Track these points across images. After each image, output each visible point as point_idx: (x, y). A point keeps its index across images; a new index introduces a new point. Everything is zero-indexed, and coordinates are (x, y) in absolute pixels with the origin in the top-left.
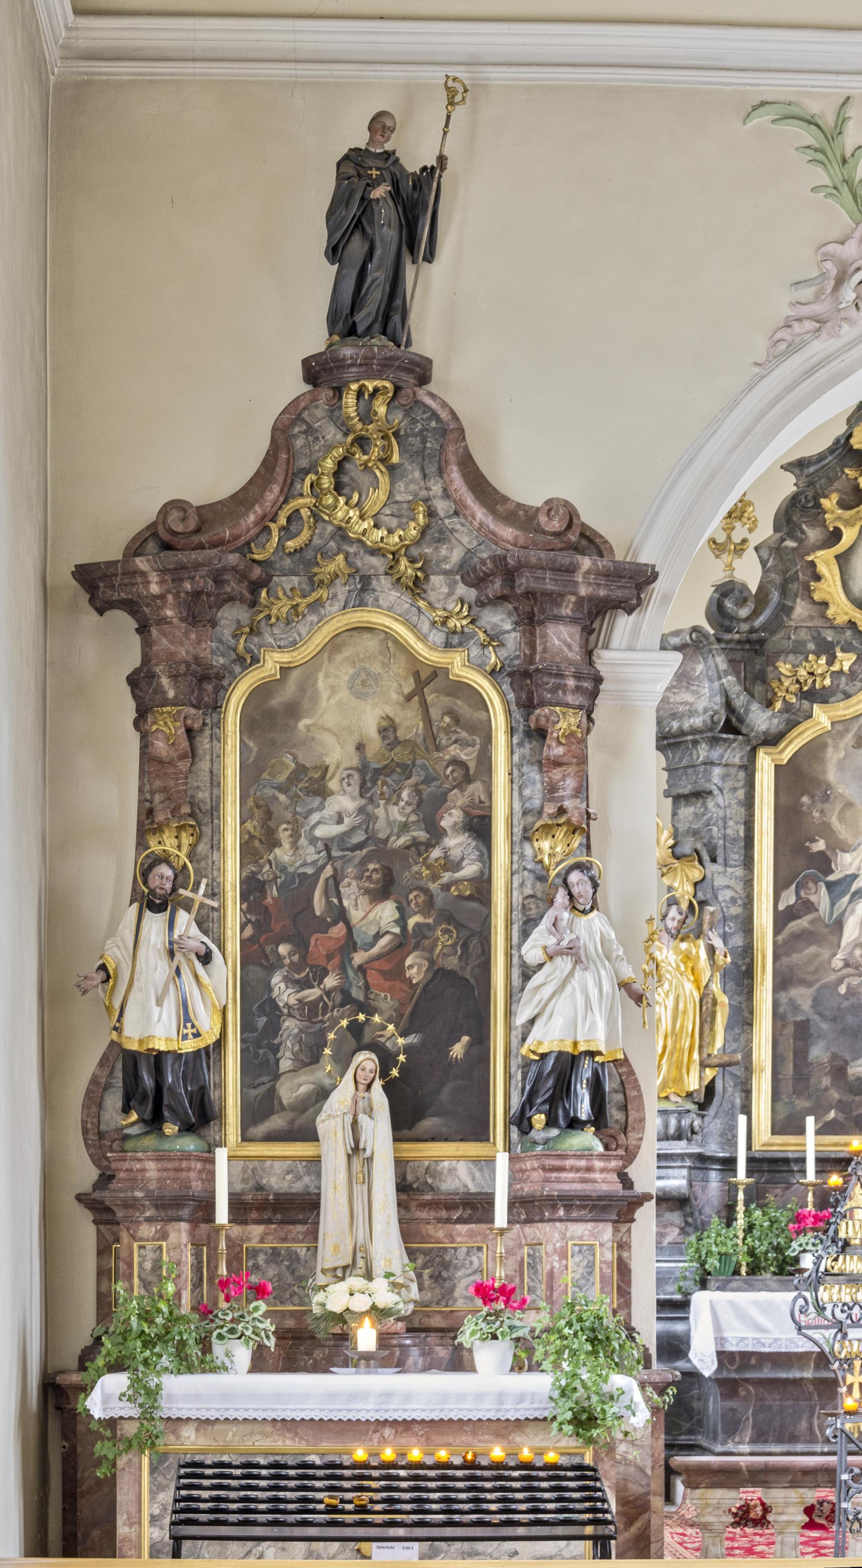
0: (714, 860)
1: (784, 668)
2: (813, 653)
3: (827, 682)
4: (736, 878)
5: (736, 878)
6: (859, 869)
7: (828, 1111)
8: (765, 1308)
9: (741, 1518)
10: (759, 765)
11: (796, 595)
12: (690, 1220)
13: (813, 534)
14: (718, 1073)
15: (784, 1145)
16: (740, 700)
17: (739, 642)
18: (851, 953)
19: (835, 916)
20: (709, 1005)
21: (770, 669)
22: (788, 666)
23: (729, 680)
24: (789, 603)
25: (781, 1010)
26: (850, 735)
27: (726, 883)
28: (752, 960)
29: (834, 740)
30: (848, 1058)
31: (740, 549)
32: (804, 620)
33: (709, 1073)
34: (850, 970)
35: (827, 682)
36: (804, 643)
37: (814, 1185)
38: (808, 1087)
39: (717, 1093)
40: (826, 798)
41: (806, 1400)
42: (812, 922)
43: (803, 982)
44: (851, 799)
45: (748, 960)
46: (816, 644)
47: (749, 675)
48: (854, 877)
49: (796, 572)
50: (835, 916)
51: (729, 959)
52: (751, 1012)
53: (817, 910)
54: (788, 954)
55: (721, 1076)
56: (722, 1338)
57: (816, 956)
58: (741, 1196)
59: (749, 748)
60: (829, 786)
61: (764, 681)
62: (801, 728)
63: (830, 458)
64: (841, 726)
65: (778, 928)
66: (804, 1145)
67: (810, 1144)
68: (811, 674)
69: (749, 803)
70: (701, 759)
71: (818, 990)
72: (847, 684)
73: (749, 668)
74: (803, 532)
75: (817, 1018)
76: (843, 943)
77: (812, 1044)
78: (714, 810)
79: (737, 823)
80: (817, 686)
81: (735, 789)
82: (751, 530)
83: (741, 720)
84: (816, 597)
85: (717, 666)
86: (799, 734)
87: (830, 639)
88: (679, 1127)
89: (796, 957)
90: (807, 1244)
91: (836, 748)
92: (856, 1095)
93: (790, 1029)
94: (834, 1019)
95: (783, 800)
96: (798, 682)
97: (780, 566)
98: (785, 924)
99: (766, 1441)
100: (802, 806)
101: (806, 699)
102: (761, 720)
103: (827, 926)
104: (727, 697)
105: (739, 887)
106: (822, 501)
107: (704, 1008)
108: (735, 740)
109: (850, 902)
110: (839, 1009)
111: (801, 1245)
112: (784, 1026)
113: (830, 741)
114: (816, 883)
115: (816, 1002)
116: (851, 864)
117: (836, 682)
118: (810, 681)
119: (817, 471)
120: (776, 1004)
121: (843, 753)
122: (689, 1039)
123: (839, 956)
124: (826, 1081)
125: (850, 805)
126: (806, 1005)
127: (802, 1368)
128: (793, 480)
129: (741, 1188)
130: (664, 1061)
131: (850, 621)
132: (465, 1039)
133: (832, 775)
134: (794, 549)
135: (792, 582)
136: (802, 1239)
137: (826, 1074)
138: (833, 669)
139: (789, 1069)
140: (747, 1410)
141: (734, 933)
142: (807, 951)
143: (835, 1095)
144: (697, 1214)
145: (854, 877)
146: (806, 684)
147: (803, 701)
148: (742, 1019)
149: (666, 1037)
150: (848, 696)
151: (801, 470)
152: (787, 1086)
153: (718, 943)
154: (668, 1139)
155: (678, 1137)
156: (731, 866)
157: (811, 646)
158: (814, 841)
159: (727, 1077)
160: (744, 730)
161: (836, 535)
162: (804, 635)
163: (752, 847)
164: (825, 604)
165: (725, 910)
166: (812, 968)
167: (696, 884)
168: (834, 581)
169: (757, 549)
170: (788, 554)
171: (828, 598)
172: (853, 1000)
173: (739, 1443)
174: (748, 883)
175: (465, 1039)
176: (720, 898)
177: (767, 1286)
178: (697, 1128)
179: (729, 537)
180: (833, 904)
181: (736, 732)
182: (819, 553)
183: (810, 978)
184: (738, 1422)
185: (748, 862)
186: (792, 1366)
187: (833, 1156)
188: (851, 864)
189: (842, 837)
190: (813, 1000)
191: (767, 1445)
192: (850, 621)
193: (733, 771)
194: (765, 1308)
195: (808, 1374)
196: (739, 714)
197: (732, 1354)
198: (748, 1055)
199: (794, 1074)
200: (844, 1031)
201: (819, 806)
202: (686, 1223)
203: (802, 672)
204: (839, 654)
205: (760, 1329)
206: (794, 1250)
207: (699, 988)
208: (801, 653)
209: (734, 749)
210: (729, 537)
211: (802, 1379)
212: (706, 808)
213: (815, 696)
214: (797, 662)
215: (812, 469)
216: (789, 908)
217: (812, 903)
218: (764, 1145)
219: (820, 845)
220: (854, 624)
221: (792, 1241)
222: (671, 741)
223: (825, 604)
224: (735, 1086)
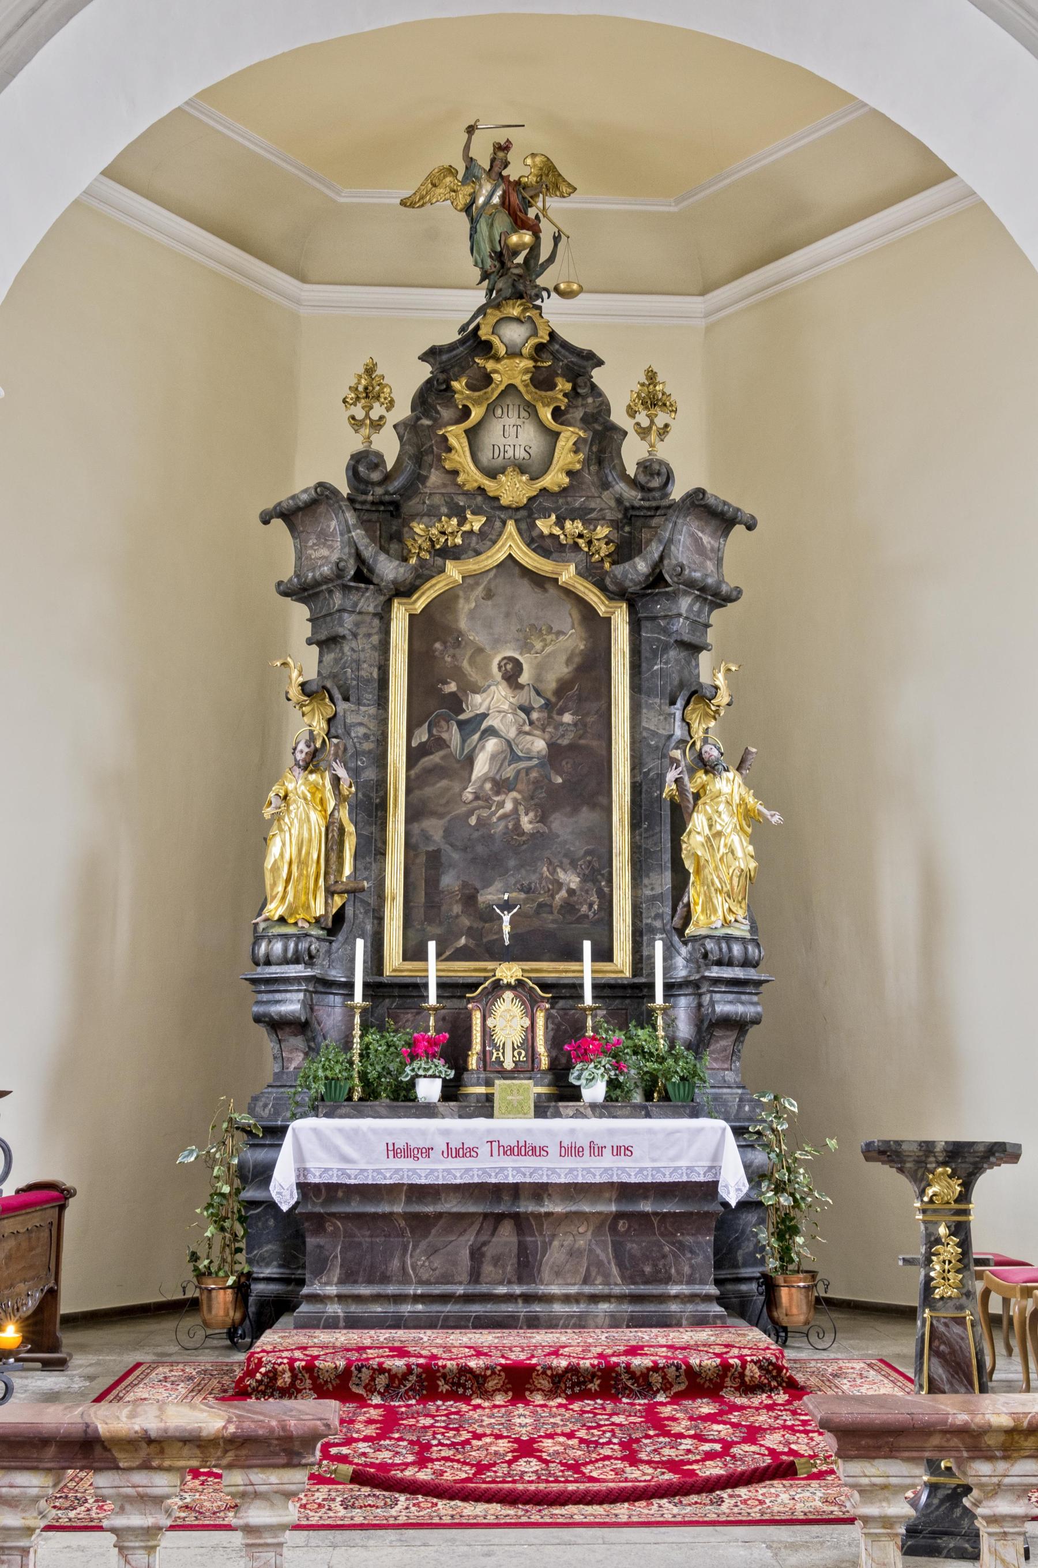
0: (346, 699)
1: (419, 528)
2: (446, 516)
3: (459, 541)
4: (369, 716)
5: (369, 716)
6: (489, 709)
8: (351, 1136)
9: (267, 1387)
10: (394, 615)
11: (431, 466)
12: (312, 1044)
13: (446, 414)
14: (348, 900)
15: (409, 970)
16: (369, 551)
17: (373, 503)
18: (481, 787)
19: (466, 752)
21: (406, 529)
23: (358, 534)
24: (424, 473)
25: (414, 840)
26: (481, 588)
28: (386, 793)
29: (465, 592)
30: (478, 885)
31: (377, 425)
32: (438, 487)
33: (338, 901)
36: (438, 507)
37: (435, 1009)
40: (458, 644)
41: (398, 1236)
42: (443, 758)
43: (434, 814)
47: (383, 533)
48: (484, 716)
49: (431, 446)
50: (466, 752)
51: (353, 789)
54: (420, 788)
56: (305, 1169)
57: (447, 789)
58: (357, 1020)
60: (460, 633)
62: (433, 581)
63: (461, 349)
64: (471, 580)
65: (410, 764)
67: (432, 970)
68: (443, 533)
69: (384, 647)
71: (449, 821)
72: (477, 543)
74: (438, 412)
76: (474, 777)
77: (443, 873)
79: (370, 666)
81: (369, 635)
82: (388, 409)
83: (371, 570)
84: (448, 466)
85: (346, 521)
87: (461, 504)
88: (296, 950)
89: (428, 791)
92: (486, 922)
93: (422, 859)
94: (465, 849)
96: (431, 540)
97: (415, 440)
98: (418, 761)
99: (355, 1282)
101: (439, 556)
102: (388, 569)
103: (458, 761)
105: (372, 725)
106: (453, 383)
107: (330, 836)
109: (481, 739)
110: (469, 839)
112: (416, 856)
113: (461, 593)
114: (448, 722)
115: (448, 833)
116: (481, 704)
117: (467, 541)
119: (449, 360)
121: (474, 604)
122: (314, 865)
123: (469, 790)
124: (457, 909)
125: (480, 650)
126: (437, 836)
127: (392, 1202)
128: (430, 369)
129: (358, 1011)
130: (289, 888)
131: (479, 488)
132: (507, 943)
133: (463, 624)
134: (429, 427)
135: (427, 454)
137: (457, 902)
138: (463, 529)
139: (421, 897)
140: (335, 1247)
141: (366, 767)
142: (439, 785)
143: (466, 922)
144: (320, 1038)
145: (484, 716)
147: (437, 558)
148: (372, 849)
149: (290, 864)
150: (478, 553)
151: (435, 359)
152: (419, 913)
153: (342, 773)
154: (288, 964)
155: (296, 960)
156: (364, 705)
157: (444, 510)
158: (446, 683)
159: (358, 904)
160: (375, 580)
161: (466, 413)
162: (437, 500)
164: (455, 473)
165: (358, 745)
166: (443, 801)
168: (464, 452)
169: (395, 427)
170: (423, 431)
171: (458, 467)
173: (326, 1284)
174: (383, 722)
175: (507, 943)
176: (353, 735)
178: (314, 952)
179: (367, 415)
180: (464, 741)
181: (368, 581)
182: (450, 428)
183: (441, 810)
184: (326, 1259)
185: (382, 702)
186: (382, 1199)
188: (481, 704)
191: (357, 1286)
192: (479, 488)
193: (368, 618)
194: (351, 1136)
195: (398, 1209)
197: (317, 1187)
199: (426, 902)
200: (473, 860)
201: (451, 651)
202: (309, 1047)
203: (434, 531)
205: (345, 1159)
206: (407, 1075)
207: (325, 818)
209: (368, 598)
210: (367, 415)
211: (391, 1214)
212: (343, 653)
213: (450, 553)
215: (445, 357)
216: (422, 745)
217: (444, 741)
218: (394, 971)
219: (452, 687)
220: (484, 490)
222: (311, 592)
223: (455, 473)
224: (366, 912)
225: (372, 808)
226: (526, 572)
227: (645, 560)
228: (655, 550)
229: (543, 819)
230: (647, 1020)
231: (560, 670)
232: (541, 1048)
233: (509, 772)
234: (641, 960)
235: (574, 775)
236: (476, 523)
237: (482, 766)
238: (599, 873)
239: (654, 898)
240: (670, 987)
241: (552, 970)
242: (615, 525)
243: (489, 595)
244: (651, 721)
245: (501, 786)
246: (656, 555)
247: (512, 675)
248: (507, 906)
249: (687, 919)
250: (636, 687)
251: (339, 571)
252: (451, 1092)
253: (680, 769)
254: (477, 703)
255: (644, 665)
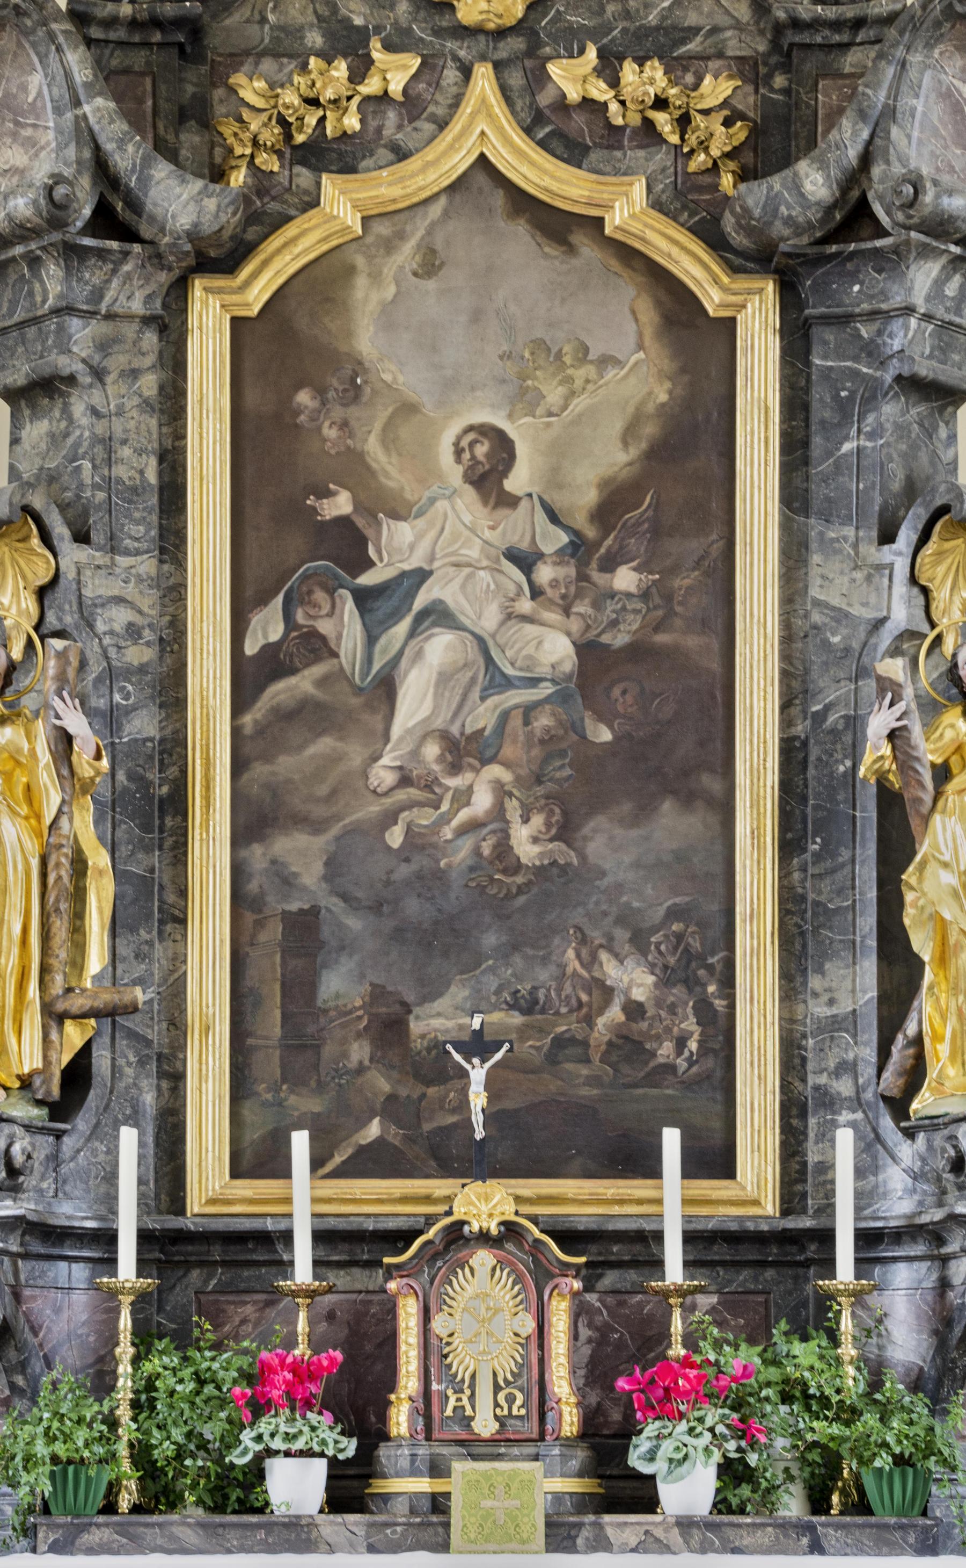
1: (251, 89)
3: (352, 122)
4: (140, 580)
5: (140, 580)
6: (432, 558)
7: (363, 1123)
10: (193, 320)
12: (20, 1380)
14: (98, 1033)
15: (247, 1200)
16: (126, 156)
17: (134, 24)
18: (415, 754)
19: (376, 667)
20: (65, 873)
21: (219, 93)
22: (260, 84)
23: (98, 109)
25: (253, 887)
26: (408, 247)
27: (116, 592)
28: (184, 772)
29: (370, 258)
30: (410, 998)
33: (74, 1036)
34: (413, 793)
35: (352, 122)
36: (297, 32)
37: (311, 1294)
38: (316, 1067)
39: (96, 1081)
40: (353, 394)
42: (322, 682)
43: (301, 821)
44: (412, 397)
45: (173, 772)
46: (329, 35)
48: (421, 576)
50: (376, 667)
52: (183, 893)
53: (335, 655)
54: (267, 758)
55: (107, 1039)
57: (335, 759)
58: (125, 1321)
59: (164, 278)
60: (359, 366)
61: (206, 124)
62: (290, 230)
66: (659, 1202)
67: (303, 1199)
68: (313, 102)
69: (172, 403)
70: (50, 301)
71: (337, 839)
72: (400, 127)
73: (163, 88)
75: (336, 904)
76: (396, 730)
77: (325, 966)
78: (84, 421)
79: (139, 452)
80: (329, 132)
81: (134, 374)
83: (135, 206)
85: (68, 75)
86: (285, 245)
87: (358, 21)
89: (286, 765)
90: (272, 1435)
91: (376, 277)
92: (429, 1083)
93: (274, 932)
94: (376, 908)
95: (251, 398)
96: (283, 122)
100: (297, 413)
101: (304, 163)
102: (179, 203)
103: (359, 691)
104: (97, 148)
105: (148, 601)
107: (51, 879)
108: (126, 254)
110: (388, 883)
111: (259, 1439)
112: (260, 924)
113: (360, 261)
114: (331, 592)
115: (334, 868)
116: (412, 547)
117: (373, 124)
118: (311, 120)
120: (238, 872)
121: (392, 289)
122: (16, 950)
123: (385, 760)
124: (359, 1052)
125: (408, 409)
126: (311, 875)
133: (366, 341)
136: (265, 1425)
137: (359, 1035)
139: (270, 1024)
142: (312, 750)
144: (37, 1365)
145: (421, 576)
146: (300, 130)
147: (298, 169)
148: (154, 909)
150: (401, 154)
152: (269, 1063)
156: (127, 553)
157: (315, 39)
159: (122, 1043)
160: (146, 231)
163: (182, 509)
165: (112, 653)
166: (322, 790)
167: (42, 593)
172: (419, 862)
174: (174, 594)
176: (100, 627)
177: (173, 1538)
180: (371, 640)
181: (129, 235)
183: (319, 811)
185: (171, 543)
187: (370, 1225)
188: (412, 547)
189: (391, 484)
190: (327, 864)
193: (129, 330)
196: (129, 191)
198: (174, 993)
199: (284, 1037)
200: (398, 935)
201: (338, 412)
203: (290, 97)
204: (378, 54)
206: (245, 1452)
207: (39, 835)
208: (291, 56)
212: (71, 420)
214: (281, 77)
216: (270, 650)
217: (323, 639)
218: (212, 1201)
219: (340, 504)
221: (243, 1427)
225: (151, 808)
226: (522, 203)
227: (823, 165)
228: (849, 138)
229: (565, 831)
230: (815, 1319)
231: (609, 456)
232: (562, 1386)
233: (482, 716)
234: (800, 1175)
235: (643, 723)
236: (395, 72)
237: (415, 703)
238: (700, 964)
239: (835, 1025)
240: (868, 1239)
241: (586, 1198)
242: (749, 70)
243: (430, 265)
244: (831, 583)
245: (463, 751)
246: (853, 154)
247: (489, 471)
248: (479, 1046)
249: (915, 1076)
250: (795, 499)
251: (56, 211)
252: (349, 1490)
253: (900, 707)
254: (398, 546)
255: (817, 441)
